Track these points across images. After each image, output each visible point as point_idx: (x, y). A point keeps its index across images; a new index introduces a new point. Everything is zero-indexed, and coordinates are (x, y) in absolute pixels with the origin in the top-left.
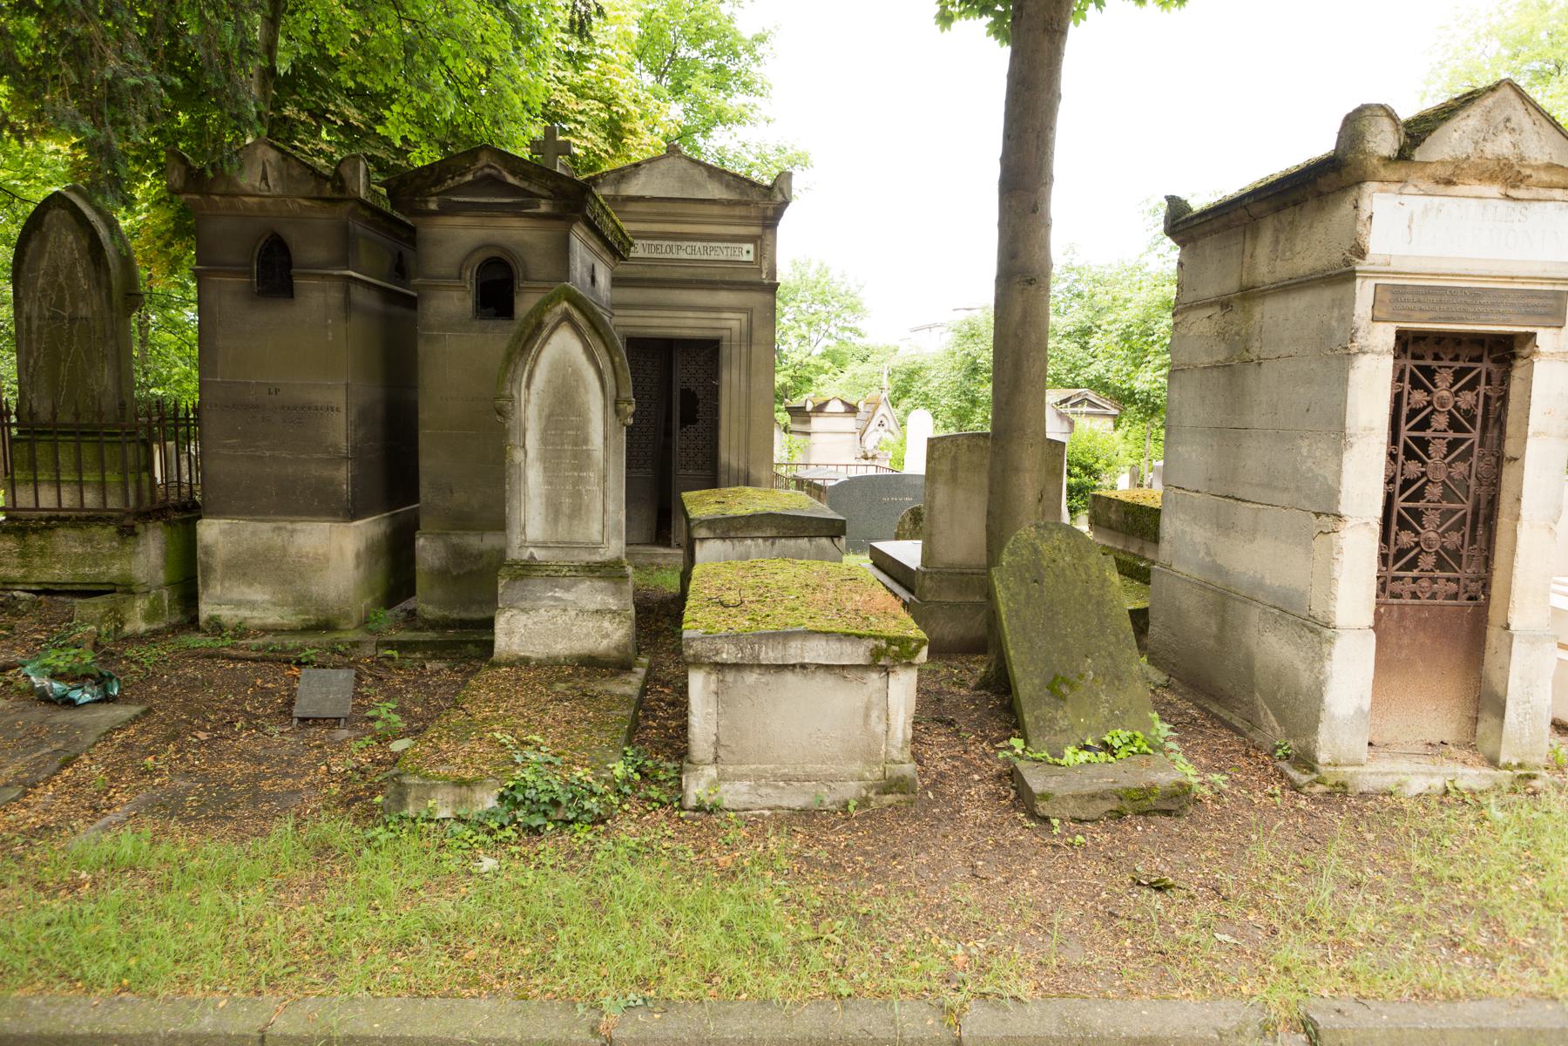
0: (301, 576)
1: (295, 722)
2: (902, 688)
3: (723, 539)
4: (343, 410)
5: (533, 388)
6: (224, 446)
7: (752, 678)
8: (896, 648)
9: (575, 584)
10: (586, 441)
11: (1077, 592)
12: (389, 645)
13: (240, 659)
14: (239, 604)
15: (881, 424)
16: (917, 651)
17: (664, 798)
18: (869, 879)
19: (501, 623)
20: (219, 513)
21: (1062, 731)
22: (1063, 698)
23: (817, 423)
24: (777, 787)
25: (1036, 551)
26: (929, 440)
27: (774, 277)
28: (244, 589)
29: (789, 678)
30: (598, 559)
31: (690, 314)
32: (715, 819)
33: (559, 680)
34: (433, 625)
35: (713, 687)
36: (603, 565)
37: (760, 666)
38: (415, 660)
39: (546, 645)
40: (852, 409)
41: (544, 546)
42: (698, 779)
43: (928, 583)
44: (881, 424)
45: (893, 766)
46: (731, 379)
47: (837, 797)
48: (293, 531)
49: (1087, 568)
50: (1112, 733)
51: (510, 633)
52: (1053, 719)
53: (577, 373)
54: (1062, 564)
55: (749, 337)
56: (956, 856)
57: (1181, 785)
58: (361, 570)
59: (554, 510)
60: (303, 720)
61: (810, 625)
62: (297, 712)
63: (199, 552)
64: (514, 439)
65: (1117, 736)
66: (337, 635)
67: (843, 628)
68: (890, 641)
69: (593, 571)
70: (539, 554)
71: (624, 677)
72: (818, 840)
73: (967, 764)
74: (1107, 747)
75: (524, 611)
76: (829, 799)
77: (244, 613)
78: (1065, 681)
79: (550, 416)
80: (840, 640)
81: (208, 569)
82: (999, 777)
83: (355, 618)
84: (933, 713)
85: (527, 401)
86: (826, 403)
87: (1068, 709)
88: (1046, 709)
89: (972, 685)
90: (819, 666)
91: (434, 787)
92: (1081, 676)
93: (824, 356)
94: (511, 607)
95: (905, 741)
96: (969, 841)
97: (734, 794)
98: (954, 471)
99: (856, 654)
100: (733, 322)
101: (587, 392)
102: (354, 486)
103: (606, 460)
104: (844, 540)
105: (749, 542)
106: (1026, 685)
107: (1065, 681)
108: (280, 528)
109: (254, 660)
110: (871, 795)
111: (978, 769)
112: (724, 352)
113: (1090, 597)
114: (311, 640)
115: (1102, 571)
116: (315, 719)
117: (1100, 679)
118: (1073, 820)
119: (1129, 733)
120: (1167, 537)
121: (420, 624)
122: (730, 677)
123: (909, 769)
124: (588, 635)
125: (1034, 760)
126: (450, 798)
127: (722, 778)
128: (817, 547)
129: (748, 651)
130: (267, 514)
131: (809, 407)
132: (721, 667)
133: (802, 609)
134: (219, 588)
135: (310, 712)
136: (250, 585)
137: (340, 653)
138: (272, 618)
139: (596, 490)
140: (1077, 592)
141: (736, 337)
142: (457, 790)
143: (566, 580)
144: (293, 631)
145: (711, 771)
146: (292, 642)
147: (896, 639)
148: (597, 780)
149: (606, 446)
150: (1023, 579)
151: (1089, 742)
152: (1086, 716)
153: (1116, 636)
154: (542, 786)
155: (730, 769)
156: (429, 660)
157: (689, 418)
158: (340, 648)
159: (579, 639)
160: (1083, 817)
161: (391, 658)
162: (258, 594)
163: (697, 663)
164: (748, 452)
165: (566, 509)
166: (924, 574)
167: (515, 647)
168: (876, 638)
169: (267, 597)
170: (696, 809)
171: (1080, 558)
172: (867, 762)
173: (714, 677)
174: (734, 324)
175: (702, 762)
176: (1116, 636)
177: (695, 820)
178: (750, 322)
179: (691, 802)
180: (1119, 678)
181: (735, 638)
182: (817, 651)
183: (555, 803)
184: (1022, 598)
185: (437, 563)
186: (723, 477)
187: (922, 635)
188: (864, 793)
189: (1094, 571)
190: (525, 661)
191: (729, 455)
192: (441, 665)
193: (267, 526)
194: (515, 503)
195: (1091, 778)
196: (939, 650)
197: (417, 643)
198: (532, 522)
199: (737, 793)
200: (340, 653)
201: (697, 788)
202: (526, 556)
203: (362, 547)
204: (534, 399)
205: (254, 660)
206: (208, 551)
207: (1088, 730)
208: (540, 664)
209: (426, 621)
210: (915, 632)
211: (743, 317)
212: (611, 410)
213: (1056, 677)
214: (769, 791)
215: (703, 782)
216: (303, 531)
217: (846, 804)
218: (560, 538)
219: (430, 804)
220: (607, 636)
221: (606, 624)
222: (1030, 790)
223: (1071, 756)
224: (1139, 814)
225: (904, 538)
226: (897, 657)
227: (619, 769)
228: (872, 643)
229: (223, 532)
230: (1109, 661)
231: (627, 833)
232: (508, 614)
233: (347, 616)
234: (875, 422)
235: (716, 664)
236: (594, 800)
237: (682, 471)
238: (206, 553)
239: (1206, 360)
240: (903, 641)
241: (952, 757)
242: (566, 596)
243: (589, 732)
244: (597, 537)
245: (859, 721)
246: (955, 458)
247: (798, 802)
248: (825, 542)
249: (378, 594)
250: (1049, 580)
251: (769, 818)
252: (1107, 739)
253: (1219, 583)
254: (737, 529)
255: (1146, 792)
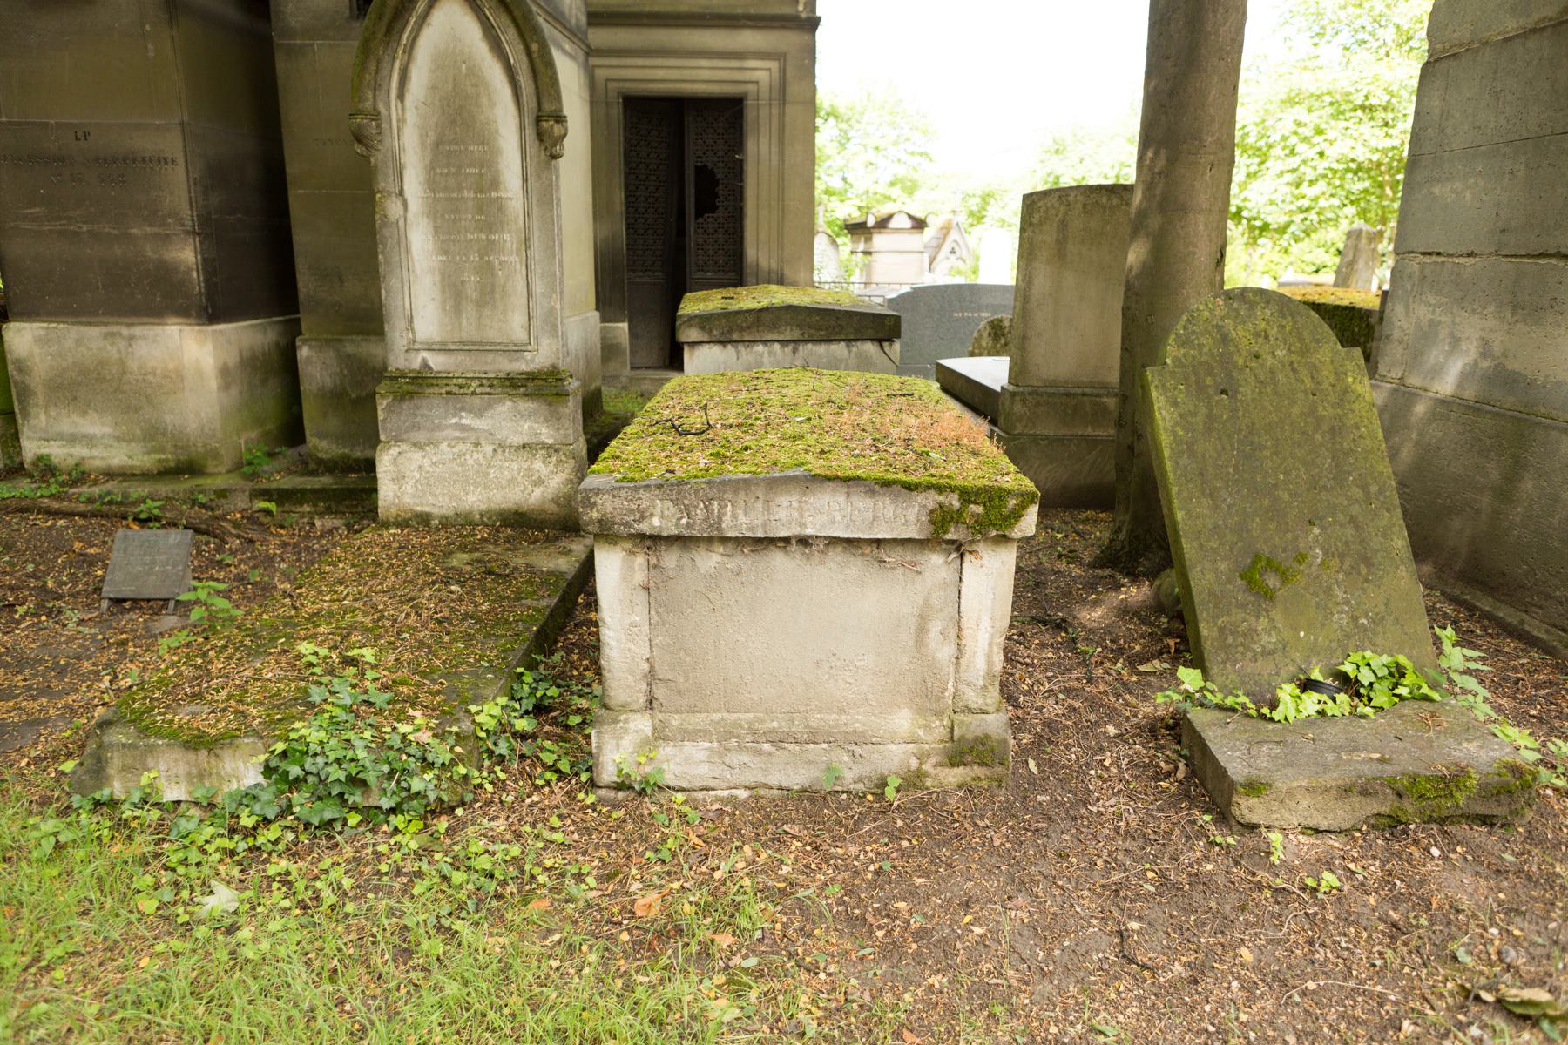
0: (149, 401)
1: (105, 604)
2: (989, 579)
3: (723, 343)
4: (181, 161)
5: (410, 99)
6: (25, 217)
7: (709, 561)
8: (979, 509)
9: (489, 406)
10: (495, 184)
11: (1295, 411)
12: (266, 494)
13: (57, 514)
14: (72, 439)
15: (953, 252)
16: (1017, 515)
17: (564, 766)
18: (918, 958)
19: (385, 464)
20: (30, 314)
21: (1266, 653)
22: (1269, 595)
23: (880, 241)
24: (759, 753)
25: (1225, 339)
26: (1025, 197)
27: (813, 10)
28: (76, 418)
29: (777, 558)
30: (523, 367)
31: (704, 63)
32: (649, 806)
33: (463, 548)
34: (330, 467)
35: (640, 577)
36: (531, 377)
37: (724, 540)
38: (303, 515)
39: (452, 497)
40: (919, 224)
41: (442, 348)
42: (618, 738)
43: (1018, 408)
44: (953, 252)
45: (967, 718)
46: (759, 150)
47: (865, 770)
48: (131, 338)
49: (1314, 369)
50: (1356, 657)
51: (399, 478)
52: (1250, 633)
53: (474, 73)
54: (1270, 361)
55: (781, 93)
56: (1086, 905)
57: (1516, 770)
58: (234, 391)
59: (453, 293)
60: (118, 602)
61: (817, 465)
62: (108, 591)
63: (10, 368)
64: (385, 183)
65: (1367, 664)
66: (200, 481)
67: (879, 472)
68: (967, 495)
69: (515, 386)
70: (437, 362)
71: (564, 543)
72: (826, 859)
73: (1094, 703)
74: (1348, 684)
75: (417, 445)
76: (851, 774)
77: (80, 451)
78: (1272, 566)
79: (438, 144)
80: (871, 493)
81: (25, 393)
82: (1153, 731)
83: (228, 460)
84: (1038, 609)
85: (402, 121)
86: (890, 217)
87: (1276, 614)
88: (1237, 614)
89: (1087, 558)
90: (833, 541)
91: (151, 749)
92: (1301, 557)
93: (892, 184)
94: (398, 440)
95: (989, 674)
96: (1108, 871)
97: (684, 763)
98: (1061, 243)
99: (903, 518)
100: (760, 74)
101: (492, 105)
102: (206, 272)
103: (527, 214)
104: (897, 345)
105: (760, 348)
106: (1206, 570)
107: (1272, 566)
108: (112, 334)
109: (83, 515)
110: (927, 767)
111: (1111, 715)
112: (750, 115)
113: (1319, 420)
114: (164, 488)
115: (1339, 374)
116: (135, 601)
117: (1335, 563)
118: (1306, 830)
119: (1385, 659)
120: (1397, 334)
121: (312, 466)
122: (670, 559)
123: (996, 723)
124: (512, 481)
125: (1220, 707)
126: (182, 769)
127: (660, 735)
128: (859, 355)
129: (700, 513)
130: (95, 314)
131: (871, 222)
132: (652, 541)
133: (811, 439)
134: (43, 417)
135: (126, 591)
136: (84, 413)
137: (202, 506)
138: (118, 457)
139: (514, 260)
140: (1295, 411)
141: (764, 94)
142: (191, 756)
143: (476, 400)
144: (146, 476)
145: (641, 724)
146: (137, 490)
147: (978, 492)
148: (440, 736)
149: (526, 192)
150: (1201, 388)
151: (1316, 675)
152: (1309, 628)
153: (1364, 487)
154: (334, 750)
155: (676, 721)
156: (321, 515)
157: (706, 205)
158: (202, 498)
159: (500, 487)
160: (1324, 826)
161: (268, 512)
162: (95, 425)
163: (607, 534)
164: (781, 247)
165: (471, 292)
166: (1013, 394)
167: (407, 499)
168: (939, 489)
169: (107, 430)
170: (619, 787)
171: (1304, 352)
172: (920, 711)
173: (640, 560)
174: (762, 76)
175: (625, 708)
176: (1364, 487)
177: (615, 805)
178: (783, 71)
179: (608, 775)
180: (1368, 562)
181: (674, 488)
182: (830, 513)
183: (356, 782)
184: (1199, 420)
185: (329, 382)
186: (750, 279)
187: (1028, 485)
188: (914, 763)
189: (1327, 374)
190: (424, 519)
191: (756, 251)
192: (338, 522)
193: (94, 332)
194: (394, 282)
195: (1335, 750)
196: (1050, 505)
197: (303, 492)
198: (421, 312)
199: (688, 761)
200: (202, 506)
201: (616, 751)
202: (416, 363)
203: (232, 359)
204: (411, 117)
205: (83, 515)
206: (22, 367)
207: (1313, 651)
208: (445, 523)
209: (320, 462)
210: (1014, 479)
211: (774, 65)
212: (530, 132)
213: (1257, 558)
214: (745, 758)
215: (628, 742)
216: (144, 338)
217: (883, 784)
218: (465, 336)
219: (145, 779)
220: (540, 482)
221: (538, 465)
222: (1222, 773)
223: (1294, 705)
224: (1431, 820)
225: (980, 355)
226: (980, 527)
227: (488, 713)
228: (932, 500)
229: (38, 340)
230: (1350, 531)
231: (485, 841)
232: (394, 451)
233: (215, 454)
234: (946, 249)
235: (642, 537)
236: (429, 776)
237: (700, 275)
238: (20, 370)
239: (1511, 25)
240: (991, 496)
241: (1068, 691)
242: (478, 423)
243: (468, 638)
244: (520, 334)
245: (907, 638)
246: (1063, 224)
247: (797, 778)
248: (870, 348)
249: (270, 426)
250: (1246, 391)
251: (745, 804)
252: (1348, 668)
253: (1509, 401)
254: (742, 329)
255: (1452, 780)
